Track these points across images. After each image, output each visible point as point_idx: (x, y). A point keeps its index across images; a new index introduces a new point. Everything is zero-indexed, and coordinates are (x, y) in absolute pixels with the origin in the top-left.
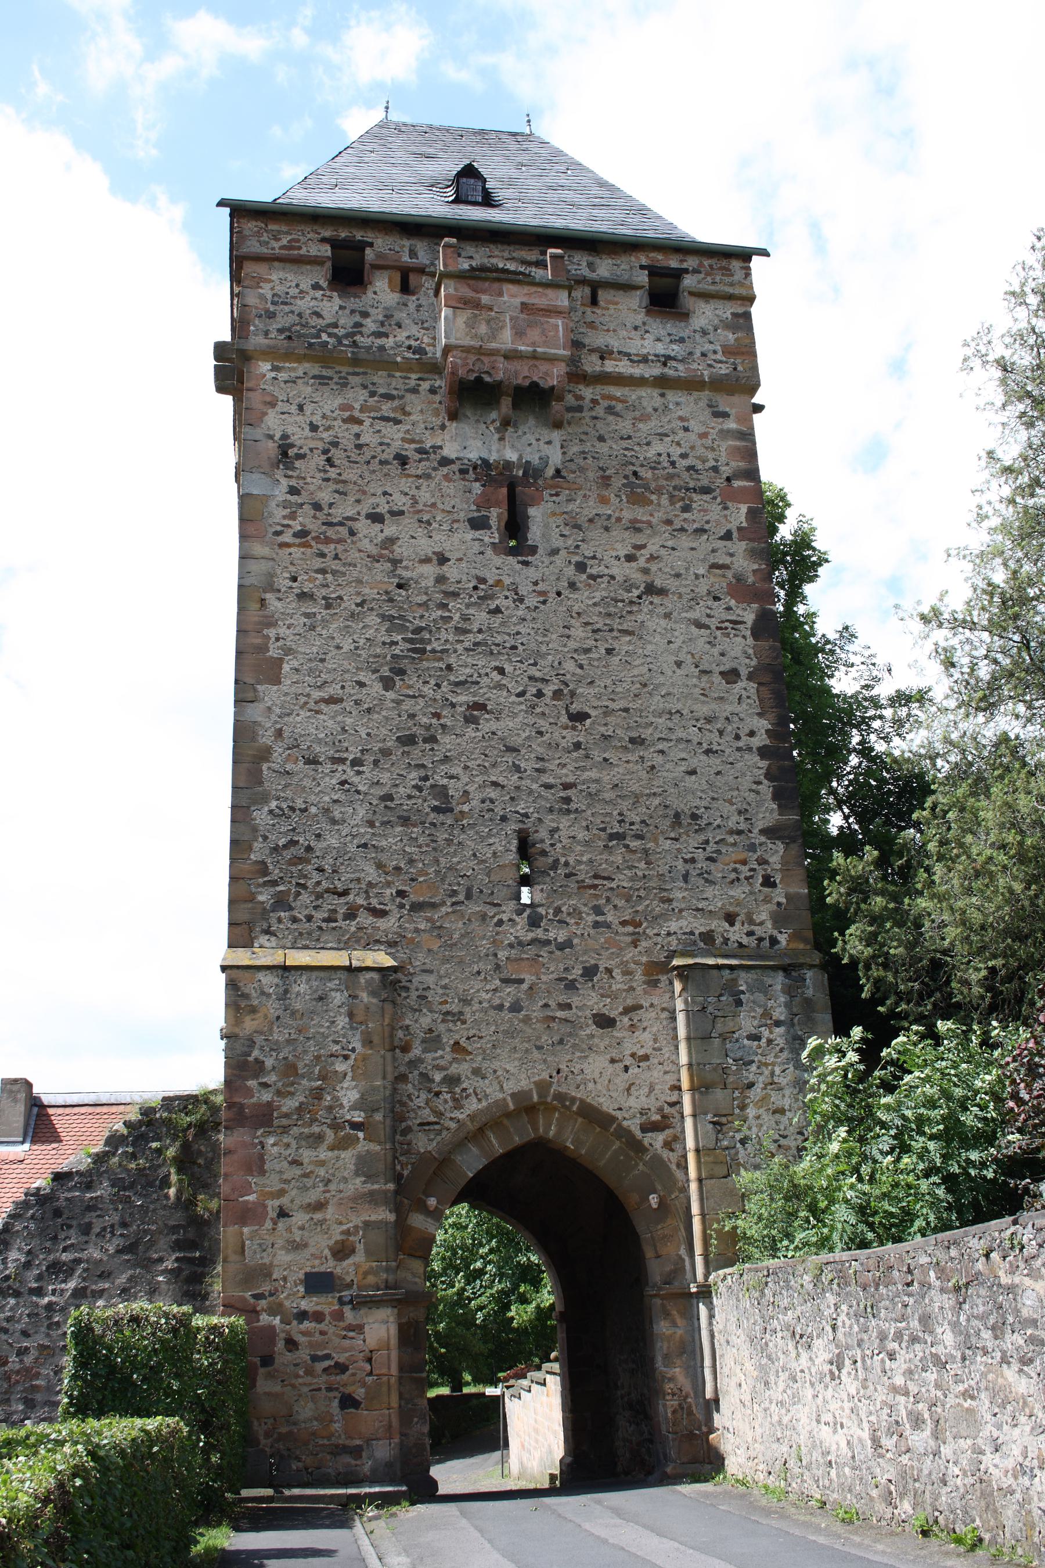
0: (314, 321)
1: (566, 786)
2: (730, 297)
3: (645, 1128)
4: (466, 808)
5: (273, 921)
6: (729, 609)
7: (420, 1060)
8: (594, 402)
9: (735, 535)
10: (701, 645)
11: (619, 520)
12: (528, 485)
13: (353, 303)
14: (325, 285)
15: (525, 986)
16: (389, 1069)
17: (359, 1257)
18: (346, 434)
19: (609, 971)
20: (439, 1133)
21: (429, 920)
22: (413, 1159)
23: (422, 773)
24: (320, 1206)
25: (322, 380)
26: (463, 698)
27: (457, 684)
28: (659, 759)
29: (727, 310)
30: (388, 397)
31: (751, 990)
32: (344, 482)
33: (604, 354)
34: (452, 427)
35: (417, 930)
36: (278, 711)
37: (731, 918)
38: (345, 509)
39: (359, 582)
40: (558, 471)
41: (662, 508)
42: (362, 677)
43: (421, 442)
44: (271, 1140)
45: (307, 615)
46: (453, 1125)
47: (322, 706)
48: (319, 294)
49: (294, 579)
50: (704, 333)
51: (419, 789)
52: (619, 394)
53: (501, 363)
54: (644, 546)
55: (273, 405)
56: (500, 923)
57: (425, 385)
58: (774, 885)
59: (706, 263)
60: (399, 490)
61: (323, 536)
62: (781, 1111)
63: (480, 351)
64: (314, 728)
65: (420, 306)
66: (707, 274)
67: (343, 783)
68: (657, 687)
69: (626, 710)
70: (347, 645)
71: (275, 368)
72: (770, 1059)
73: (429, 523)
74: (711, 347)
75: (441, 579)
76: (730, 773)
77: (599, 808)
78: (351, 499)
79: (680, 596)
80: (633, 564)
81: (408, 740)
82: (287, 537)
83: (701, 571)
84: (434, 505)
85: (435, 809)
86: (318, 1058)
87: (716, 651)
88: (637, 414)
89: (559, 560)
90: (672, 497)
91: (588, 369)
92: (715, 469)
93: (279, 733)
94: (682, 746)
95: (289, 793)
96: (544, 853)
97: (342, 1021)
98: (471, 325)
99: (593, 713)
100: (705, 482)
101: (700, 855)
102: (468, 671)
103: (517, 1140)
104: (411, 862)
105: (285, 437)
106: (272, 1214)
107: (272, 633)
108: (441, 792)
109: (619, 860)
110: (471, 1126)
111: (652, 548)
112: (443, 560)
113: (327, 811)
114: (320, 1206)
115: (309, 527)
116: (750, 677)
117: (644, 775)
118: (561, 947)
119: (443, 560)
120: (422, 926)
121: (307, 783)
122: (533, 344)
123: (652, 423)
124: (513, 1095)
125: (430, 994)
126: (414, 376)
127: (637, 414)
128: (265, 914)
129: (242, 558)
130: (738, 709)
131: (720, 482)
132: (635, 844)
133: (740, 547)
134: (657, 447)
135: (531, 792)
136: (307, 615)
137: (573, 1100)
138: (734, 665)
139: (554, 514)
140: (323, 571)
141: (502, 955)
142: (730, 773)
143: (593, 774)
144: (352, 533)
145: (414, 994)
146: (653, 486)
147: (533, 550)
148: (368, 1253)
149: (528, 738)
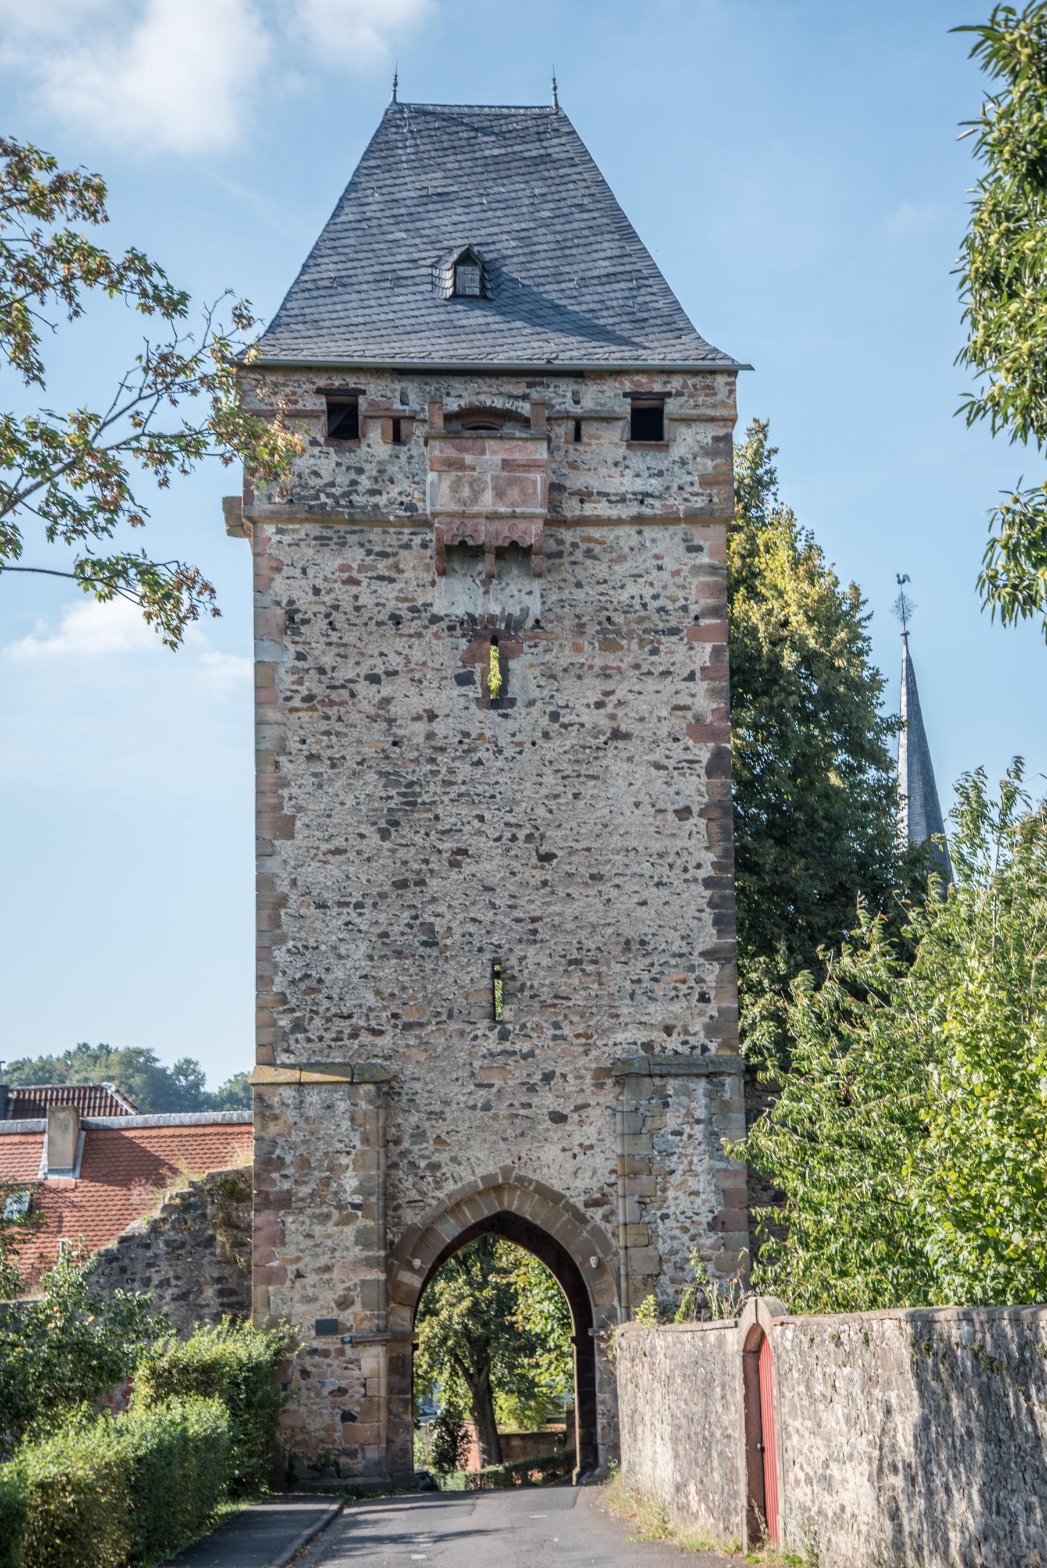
0: (314, 481)
1: (534, 920)
2: (712, 420)
3: (587, 1205)
4: (449, 942)
5: (292, 1042)
6: (687, 749)
7: (409, 1151)
8: (575, 545)
9: (698, 675)
10: (659, 784)
11: (591, 667)
12: (510, 638)
13: (349, 459)
14: (322, 440)
15: (494, 1090)
16: (382, 1161)
17: (357, 1308)
18: (344, 594)
19: (564, 1076)
20: (423, 1208)
21: (418, 1037)
22: (403, 1229)
23: (413, 912)
24: (328, 1269)
25: (323, 541)
26: (448, 845)
27: (443, 832)
28: (614, 893)
29: (706, 434)
30: (384, 555)
31: (677, 1094)
32: (345, 645)
33: (584, 496)
34: (442, 582)
35: (408, 1046)
36: (292, 863)
37: (668, 1030)
38: (346, 672)
39: (360, 742)
40: (537, 621)
41: (633, 652)
42: (364, 829)
43: (413, 600)
44: (290, 1219)
45: (315, 775)
46: (434, 1202)
47: (330, 857)
48: (316, 450)
49: (304, 742)
50: (683, 462)
51: (411, 926)
52: (597, 536)
53: (483, 526)
54: (612, 692)
55: (278, 570)
56: (476, 1038)
57: (417, 540)
58: (708, 1001)
59: (690, 382)
60: (394, 648)
61: (328, 699)
62: (697, 1193)
63: (463, 515)
64: (324, 876)
65: (411, 457)
66: (691, 396)
67: (347, 924)
68: (616, 827)
69: (588, 850)
70: (350, 801)
71: (280, 531)
72: (690, 1151)
73: (420, 682)
74: (689, 478)
75: (430, 736)
76: (677, 902)
77: (561, 938)
78: (351, 662)
79: (643, 739)
80: (602, 711)
81: (402, 884)
82: (296, 702)
83: (664, 713)
84: (424, 664)
85: (424, 944)
86: (326, 1154)
87: (671, 791)
88: (614, 555)
89: (535, 711)
90: (641, 640)
91: (568, 514)
92: (685, 609)
93: (294, 883)
94: (636, 880)
95: (303, 934)
96: (513, 978)
97: (346, 1124)
98: (455, 488)
99: (559, 853)
100: (674, 623)
101: (646, 976)
102: (453, 820)
103: (486, 1213)
104: (404, 989)
105: (291, 602)
106: (291, 1276)
107: (285, 792)
108: (429, 928)
109: (576, 982)
110: (448, 1203)
111: (620, 694)
112: (432, 716)
113: (334, 948)
114: (328, 1269)
115: (315, 691)
116: (701, 815)
117: (601, 907)
118: (525, 1057)
119: (432, 716)
120: (412, 1042)
121: (318, 925)
122: (513, 505)
123: (627, 565)
124: (483, 1178)
125: (417, 1098)
126: (406, 531)
127: (614, 555)
128: (285, 1036)
129: (258, 724)
130: (687, 843)
131: (688, 622)
132: (590, 968)
133: (701, 687)
134: (632, 589)
135: (504, 926)
136: (315, 775)
137: (531, 1181)
138: (687, 803)
139: (532, 666)
140: (328, 733)
141: (477, 1064)
142: (677, 902)
143: (557, 908)
144: (353, 695)
145: (405, 1098)
146: (624, 630)
147: (512, 702)
148: (365, 1305)
149: (503, 878)
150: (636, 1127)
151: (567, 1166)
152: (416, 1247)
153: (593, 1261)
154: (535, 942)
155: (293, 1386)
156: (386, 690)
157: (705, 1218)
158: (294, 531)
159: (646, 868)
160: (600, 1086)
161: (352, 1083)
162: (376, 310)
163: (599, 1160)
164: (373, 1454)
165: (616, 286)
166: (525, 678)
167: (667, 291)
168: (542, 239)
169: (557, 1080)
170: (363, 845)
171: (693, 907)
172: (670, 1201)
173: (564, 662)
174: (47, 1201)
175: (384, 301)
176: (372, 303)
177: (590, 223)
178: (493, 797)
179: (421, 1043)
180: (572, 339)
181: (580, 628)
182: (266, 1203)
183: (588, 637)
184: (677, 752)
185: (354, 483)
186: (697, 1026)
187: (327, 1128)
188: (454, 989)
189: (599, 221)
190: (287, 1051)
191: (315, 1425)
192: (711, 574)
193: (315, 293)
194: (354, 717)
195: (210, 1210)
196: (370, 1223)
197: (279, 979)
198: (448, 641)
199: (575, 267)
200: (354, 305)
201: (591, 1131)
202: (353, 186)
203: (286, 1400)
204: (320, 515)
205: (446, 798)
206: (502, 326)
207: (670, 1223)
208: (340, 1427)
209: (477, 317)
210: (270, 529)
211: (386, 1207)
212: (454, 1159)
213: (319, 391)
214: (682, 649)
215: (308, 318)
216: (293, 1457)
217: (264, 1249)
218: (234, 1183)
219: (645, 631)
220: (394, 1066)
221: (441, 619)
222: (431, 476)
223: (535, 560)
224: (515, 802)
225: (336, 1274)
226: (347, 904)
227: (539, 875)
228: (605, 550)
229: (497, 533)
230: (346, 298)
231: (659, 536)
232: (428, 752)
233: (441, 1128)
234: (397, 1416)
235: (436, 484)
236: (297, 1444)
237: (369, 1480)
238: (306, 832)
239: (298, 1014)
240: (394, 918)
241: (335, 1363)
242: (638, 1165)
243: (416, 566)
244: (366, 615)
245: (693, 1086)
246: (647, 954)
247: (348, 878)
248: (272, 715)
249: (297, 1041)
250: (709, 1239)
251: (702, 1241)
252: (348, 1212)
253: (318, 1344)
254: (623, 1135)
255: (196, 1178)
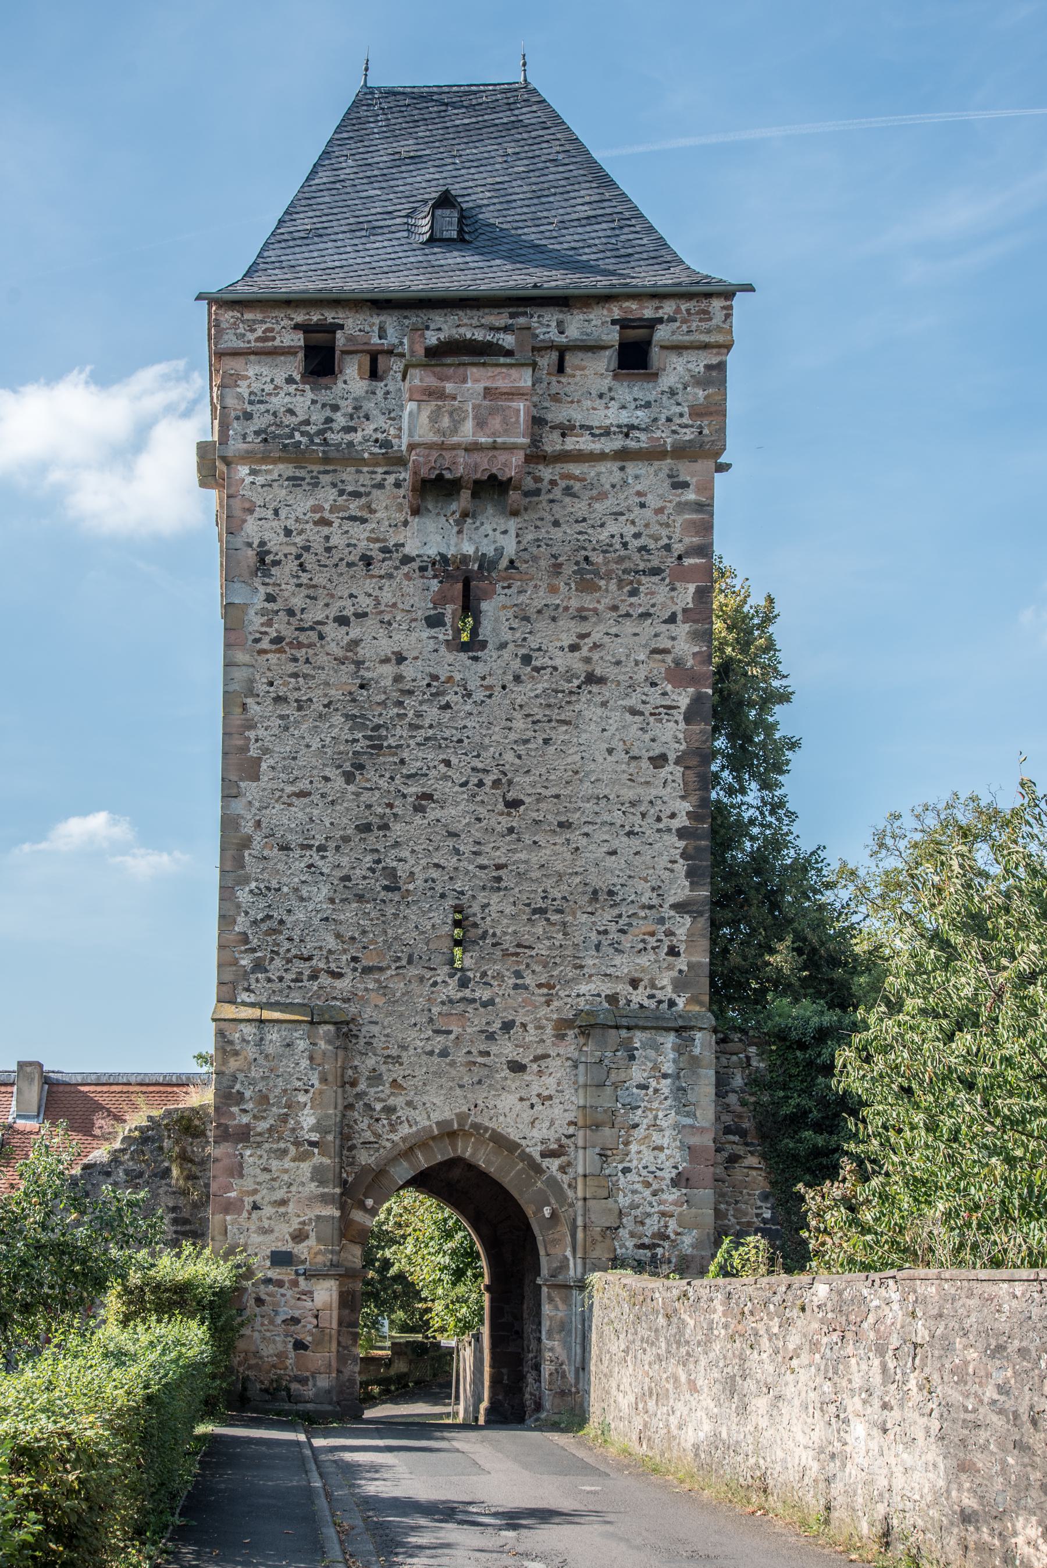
1: (499, 867)
2: (705, 346)
4: (411, 887)
5: (253, 981)
8: (553, 483)
9: (680, 617)
11: (566, 609)
12: (483, 578)
13: (325, 396)
14: (298, 378)
15: (452, 1037)
16: (340, 1101)
17: (312, 1242)
18: (314, 535)
19: (524, 1026)
20: (377, 1150)
21: (377, 981)
23: (376, 856)
24: (283, 1202)
26: (413, 789)
27: (409, 777)
28: (583, 841)
30: (356, 495)
31: (644, 1047)
32: (315, 586)
33: (566, 430)
34: (414, 521)
35: (366, 989)
36: (257, 804)
37: (634, 983)
39: (327, 684)
40: (512, 562)
41: (611, 592)
42: (328, 772)
43: (385, 540)
44: (248, 1152)
45: (281, 717)
46: (388, 1145)
47: (294, 799)
49: (271, 684)
50: (673, 393)
51: (373, 870)
52: (577, 472)
53: (461, 457)
54: (588, 635)
55: (251, 511)
57: (391, 479)
58: (678, 954)
59: (683, 307)
60: (364, 590)
61: (296, 640)
62: (660, 1149)
63: (442, 447)
64: (287, 819)
65: (388, 393)
66: (684, 321)
67: (310, 866)
68: (587, 775)
69: (557, 796)
70: (316, 744)
73: (390, 623)
74: (678, 409)
75: (398, 678)
77: (526, 886)
79: (619, 683)
80: (577, 654)
81: (366, 828)
82: (265, 644)
83: (642, 657)
84: (394, 605)
85: (386, 888)
86: (285, 1091)
87: (647, 737)
88: (595, 492)
89: (506, 654)
90: (620, 581)
92: (667, 548)
93: (258, 824)
96: (475, 925)
97: (305, 1063)
98: (434, 418)
99: (527, 800)
100: (655, 563)
101: (613, 927)
102: (419, 764)
103: (439, 1158)
105: (262, 544)
106: (248, 1207)
107: (252, 734)
108: (391, 874)
109: (540, 931)
111: (596, 637)
112: (400, 659)
113: (296, 890)
114: (283, 1202)
117: (568, 856)
118: (485, 1005)
119: (400, 659)
121: (281, 866)
122: (494, 434)
123: (608, 503)
124: (438, 1123)
125: (374, 1041)
126: (380, 470)
127: (595, 492)
128: (246, 975)
130: (662, 792)
131: (671, 561)
132: (555, 918)
134: (612, 528)
135: (467, 872)
136: (281, 717)
137: (486, 1129)
138: (663, 750)
139: (504, 607)
140: (295, 675)
141: (435, 1010)
143: (523, 856)
144: (321, 637)
145: (362, 1041)
146: (603, 570)
148: (319, 1240)
149: (468, 824)
150: (600, 1079)
151: (524, 1115)
152: (369, 1187)
153: (547, 1211)
154: (499, 889)
155: (248, 1312)
156: (355, 632)
157: (669, 1174)
158: (267, 472)
159: (617, 817)
160: (561, 1037)
161: (311, 1023)
162: (352, 255)
163: (557, 1111)
164: (324, 1382)
165: (597, 227)
166: (497, 620)
167: (650, 229)
168: (517, 190)
169: (517, 1029)
170: (327, 788)
171: (666, 858)
172: (633, 1155)
173: (538, 604)
174: (15, 1141)
175: (360, 247)
176: (349, 249)
177: (566, 175)
178: (460, 741)
179: (380, 987)
180: (554, 272)
181: (556, 569)
182: (224, 1135)
183: (564, 577)
184: (655, 697)
185: (329, 420)
186: (665, 980)
187: (286, 1066)
188: (414, 934)
189: (575, 173)
190: (247, 989)
191: (268, 1351)
192: (697, 511)
193: (291, 243)
194: (322, 659)
195: (166, 1144)
196: (327, 1161)
197: (241, 919)
198: (419, 582)
199: (553, 213)
200: (330, 251)
201: (551, 1082)
202: (326, 154)
203: (242, 1325)
204: (294, 455)
205: (412, 742)
206: (481, 264)
207: (632, 1177)
208: (292, 1354)
209: (454, 258)
210: (243, 471)
211: (342, 1147)
212: (409, 1103)
213: (297, 327)
214: (663, 590)
215: (284, 264)
216: (246, 1379)
217: (222, 1180)
218: (190, 1120)
219: (624, 571)
220: (353, 1009)
221: (413, 559)
222: (411, 406)
223: (514, 496)
224: (486, 748)
225: (291, 1208)
226: (309, 847)
227: (505, 822)
228: (585, 487)
229: (476, 466)
230: (322, 246)
231: (643, 472)
232: (395, 695)
233: (397, 1072)
234: (346, 1348)
235: (412, 418)
236: (250, 1367)
237: (319, 1407)
238: (272, 775)
239: (259, 954)
240: (354, 861)
241: (289, 1293)
242: (600, 1117)
243: (388, 504)
244: (336, 555)
245: (661, 1040)
246: (614, 905)
247: (311, 820)
248: (241, 657)
249: (257, 980)
250: (672, 1195)
251: (665, 1196)
252: (305, 1149)
253: (273, 1274)
254: (586, 1086)
255: (155, 1113)
